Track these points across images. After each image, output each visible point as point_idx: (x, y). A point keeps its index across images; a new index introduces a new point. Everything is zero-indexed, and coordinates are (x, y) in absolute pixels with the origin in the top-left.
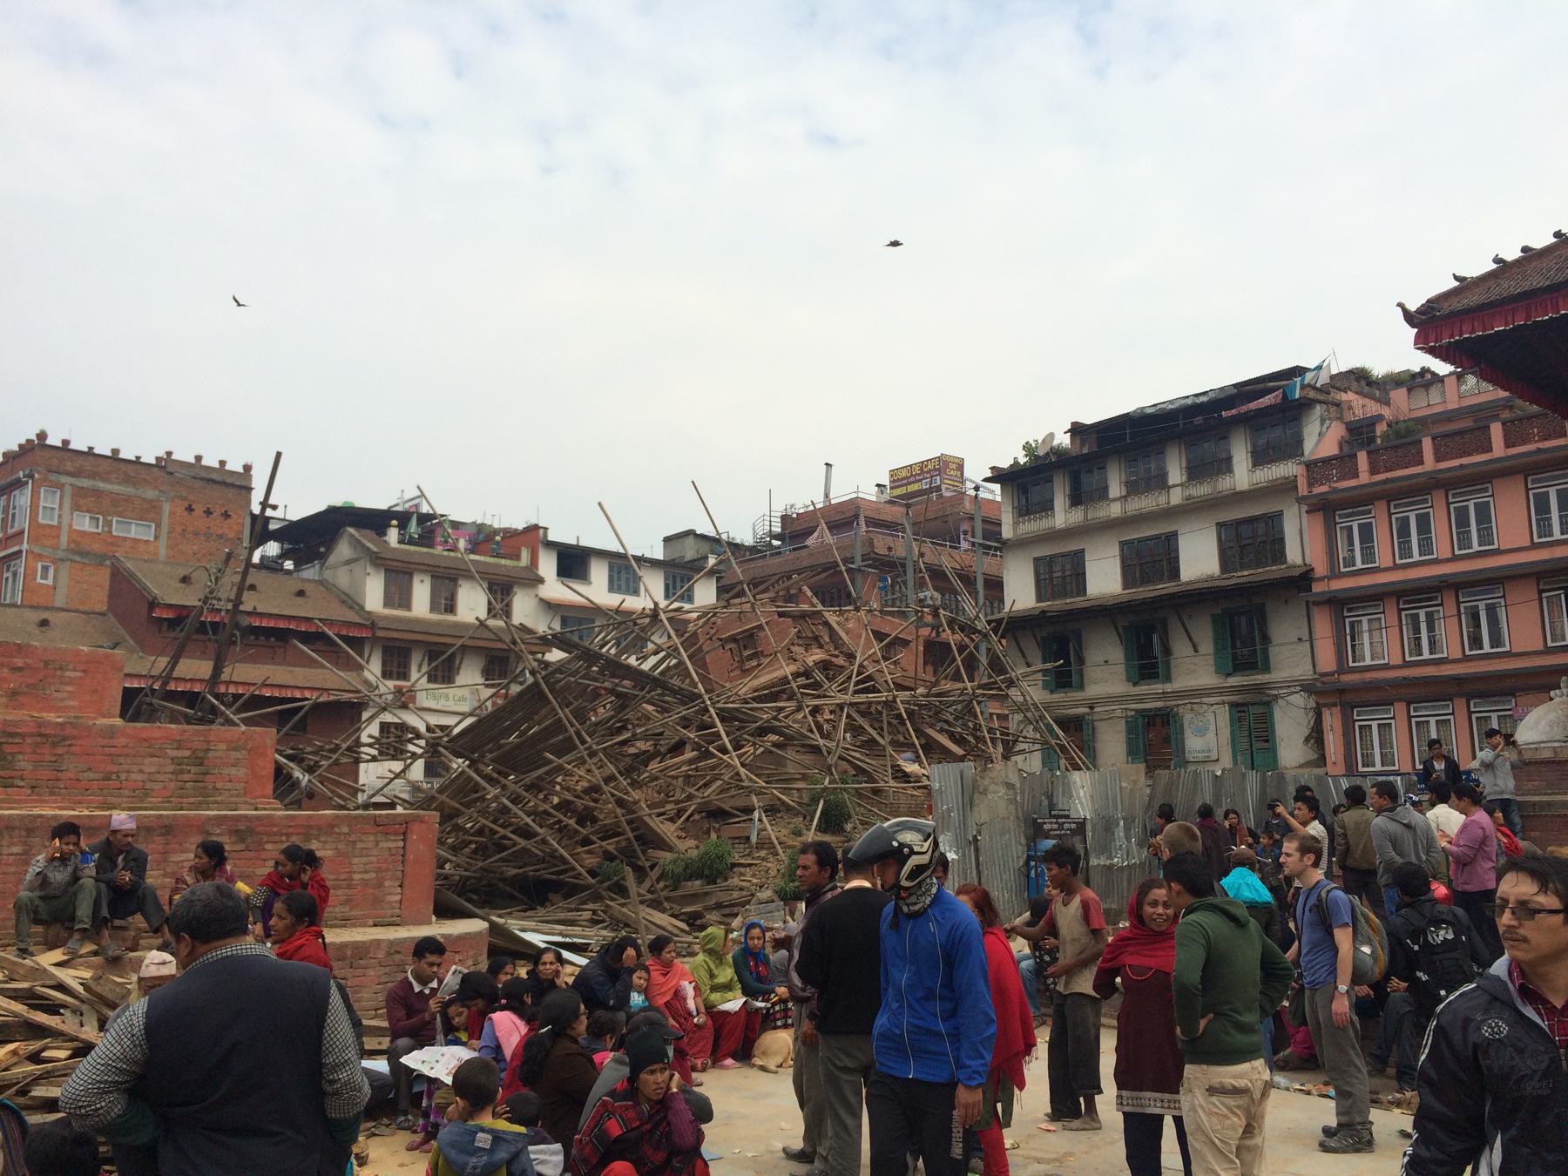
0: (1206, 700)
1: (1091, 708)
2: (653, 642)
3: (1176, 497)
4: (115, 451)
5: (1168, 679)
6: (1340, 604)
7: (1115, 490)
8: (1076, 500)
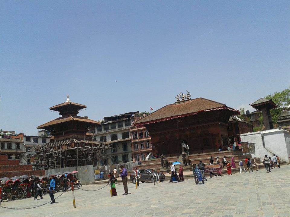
8: (105, 129)
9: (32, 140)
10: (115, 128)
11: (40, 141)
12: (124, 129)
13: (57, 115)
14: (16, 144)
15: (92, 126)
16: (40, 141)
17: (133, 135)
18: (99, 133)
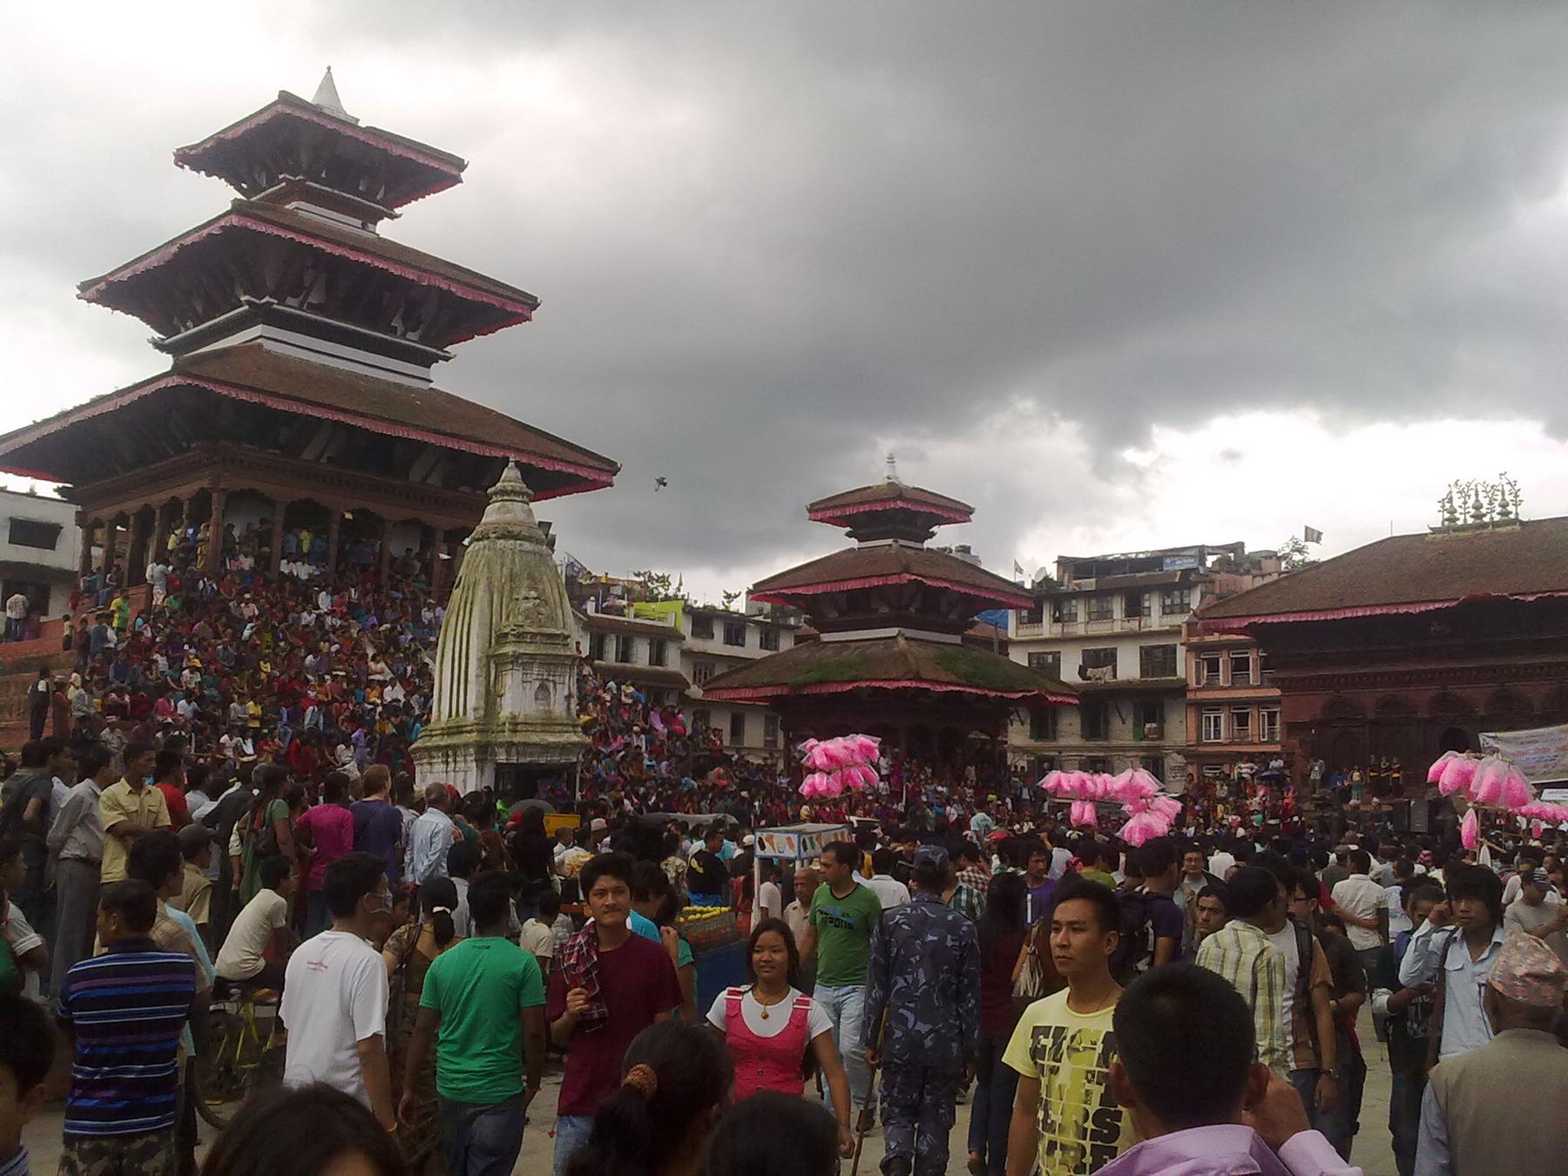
0: (1128, 754)
1: (1060, 753)
2: (491, 697)
3: (1117, 628)
4: (35, 422)
5: (1107, 738)
6: (1200, 706)
7: (1081, 617)
9: (719, 631)
10: (1106, 615)
11: (753, 639)
12: (1155, 628)
13: (834, 542)
14: (651, 645)
15: (1005, 595)
16: (753, 639)
17: (1197, 664)
18: (1028, 633)
